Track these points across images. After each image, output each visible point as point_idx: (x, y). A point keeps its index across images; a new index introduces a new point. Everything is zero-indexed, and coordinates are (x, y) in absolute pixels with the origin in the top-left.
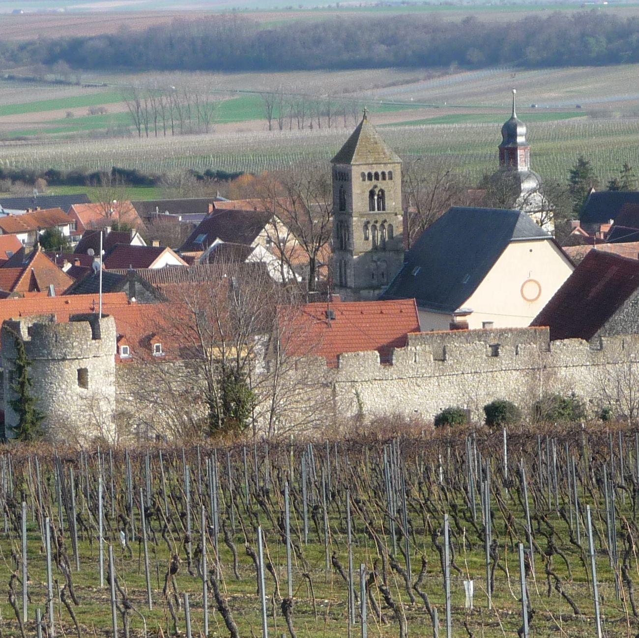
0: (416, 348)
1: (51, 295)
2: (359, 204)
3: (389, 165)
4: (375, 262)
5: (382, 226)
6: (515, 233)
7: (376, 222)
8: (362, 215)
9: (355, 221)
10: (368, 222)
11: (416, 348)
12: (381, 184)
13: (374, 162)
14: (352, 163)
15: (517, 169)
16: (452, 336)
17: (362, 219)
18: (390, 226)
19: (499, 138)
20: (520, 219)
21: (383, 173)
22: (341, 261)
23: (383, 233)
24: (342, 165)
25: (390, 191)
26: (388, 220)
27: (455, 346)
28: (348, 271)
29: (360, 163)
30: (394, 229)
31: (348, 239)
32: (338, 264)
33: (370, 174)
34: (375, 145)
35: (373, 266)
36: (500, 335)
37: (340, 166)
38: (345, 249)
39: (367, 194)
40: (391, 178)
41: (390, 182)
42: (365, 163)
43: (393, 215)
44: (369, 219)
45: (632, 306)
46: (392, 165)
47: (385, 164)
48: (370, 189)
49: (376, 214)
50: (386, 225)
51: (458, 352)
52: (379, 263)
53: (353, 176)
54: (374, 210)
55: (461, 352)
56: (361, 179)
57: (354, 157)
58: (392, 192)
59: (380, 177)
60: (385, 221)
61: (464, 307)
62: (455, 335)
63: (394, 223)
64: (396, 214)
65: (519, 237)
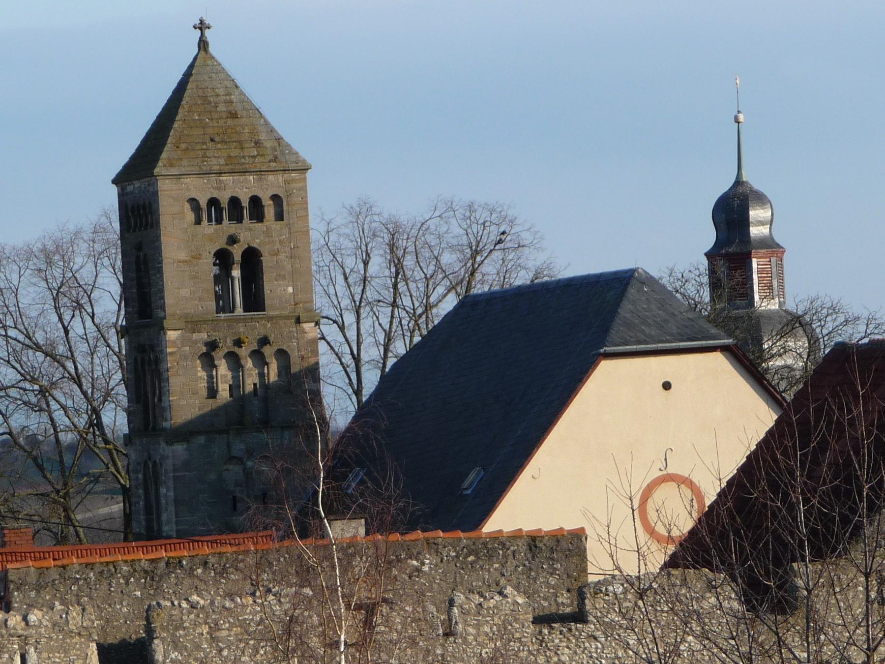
0: (25, 619)
2: (185, 292)
3: (271, 178)
4: (240, 461)
6: (617, 330)
7: (238, 343)
8: (192, 324)
9: (174, 342)
10: (212, 345)
11: (25, 619)
13: (226, 168)
14: (157, 171)
16: (191, 572)
17: (195, 336)
18: (282, 354)
19: (708, 237)
21: (255, 202)
22: (146, 463)
24: (137, 184)
25: (277, 253)
26: (271, 339)
27: (193, 606)
28: (163, 490)
31: (160, 400)
32: (140, 476)
34: (230, 122)
37: (136, 186)
38: (154, 429)
39: (207, 261)
40: (279, 216)
41: (277, 226)
44: (215, 336)
46: (280, 178)
48: (221, 244)
50: (268, 351)
51: (205, 629)
53: (162, 210)
55: (216, 627)
56: (190, 216)
57: (164, 155)
58: (282, 256)
60: (264, 341)
62: (205, 564)
64: (298, 321)
65: (626, 344)
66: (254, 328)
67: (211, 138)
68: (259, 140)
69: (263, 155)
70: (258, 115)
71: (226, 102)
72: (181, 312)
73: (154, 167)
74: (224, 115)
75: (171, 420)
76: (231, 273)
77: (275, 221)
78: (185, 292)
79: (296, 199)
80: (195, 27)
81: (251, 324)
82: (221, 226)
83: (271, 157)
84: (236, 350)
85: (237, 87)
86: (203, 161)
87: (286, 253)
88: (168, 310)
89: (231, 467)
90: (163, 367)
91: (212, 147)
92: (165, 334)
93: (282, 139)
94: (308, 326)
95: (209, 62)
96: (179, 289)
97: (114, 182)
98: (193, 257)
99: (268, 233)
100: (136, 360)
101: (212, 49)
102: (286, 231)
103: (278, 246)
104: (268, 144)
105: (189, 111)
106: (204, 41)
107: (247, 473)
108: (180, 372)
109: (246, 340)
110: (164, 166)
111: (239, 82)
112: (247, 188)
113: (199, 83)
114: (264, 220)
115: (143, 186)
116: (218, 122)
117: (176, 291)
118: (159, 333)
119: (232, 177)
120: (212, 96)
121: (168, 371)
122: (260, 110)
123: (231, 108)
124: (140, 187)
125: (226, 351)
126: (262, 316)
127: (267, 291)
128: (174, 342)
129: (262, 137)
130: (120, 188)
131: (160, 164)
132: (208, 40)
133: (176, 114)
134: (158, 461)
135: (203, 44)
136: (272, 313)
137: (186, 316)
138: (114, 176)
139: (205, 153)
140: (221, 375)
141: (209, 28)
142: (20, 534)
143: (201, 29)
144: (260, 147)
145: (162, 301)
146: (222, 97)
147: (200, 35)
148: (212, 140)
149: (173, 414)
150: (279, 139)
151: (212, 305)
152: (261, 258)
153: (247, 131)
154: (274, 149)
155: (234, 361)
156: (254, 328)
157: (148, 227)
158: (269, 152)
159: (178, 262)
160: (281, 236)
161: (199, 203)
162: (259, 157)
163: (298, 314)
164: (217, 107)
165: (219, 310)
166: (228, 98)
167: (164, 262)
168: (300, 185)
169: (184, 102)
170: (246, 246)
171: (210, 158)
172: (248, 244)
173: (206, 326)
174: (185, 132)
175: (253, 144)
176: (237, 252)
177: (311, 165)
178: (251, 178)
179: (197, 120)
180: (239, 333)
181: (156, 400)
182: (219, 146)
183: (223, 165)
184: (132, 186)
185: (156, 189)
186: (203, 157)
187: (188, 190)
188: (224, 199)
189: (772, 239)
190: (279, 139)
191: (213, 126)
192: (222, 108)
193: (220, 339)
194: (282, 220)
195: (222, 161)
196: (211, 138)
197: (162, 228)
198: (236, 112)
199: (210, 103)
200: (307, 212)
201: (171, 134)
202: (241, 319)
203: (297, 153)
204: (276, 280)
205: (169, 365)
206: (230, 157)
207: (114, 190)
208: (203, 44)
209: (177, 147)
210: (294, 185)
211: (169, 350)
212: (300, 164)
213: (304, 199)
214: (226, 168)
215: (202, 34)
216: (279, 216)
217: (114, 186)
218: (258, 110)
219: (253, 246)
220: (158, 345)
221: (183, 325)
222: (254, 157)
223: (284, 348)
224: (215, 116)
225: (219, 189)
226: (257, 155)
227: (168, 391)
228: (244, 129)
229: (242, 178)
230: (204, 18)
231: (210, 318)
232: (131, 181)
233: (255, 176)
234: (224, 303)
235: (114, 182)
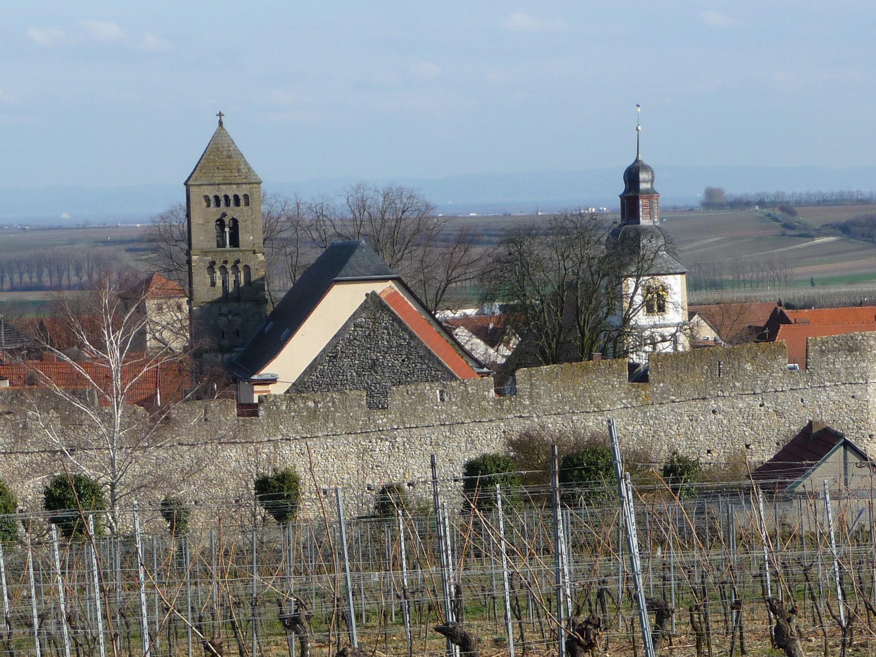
1: (440, 392)
2: (202, 238)
3: (244, 186)
5: (235, 267)
6: (346, 269)
7: (226, 262)
8: (205, 253)
9: (195, 261)
10: (213, 263)
12: (233, 212)
13: (222, 182)
15: (639, 223)
18: (247, 267)
19: (621, 187)
20: (357, 251)
21: (236, 198)
23: (237, 277)
26: (241, 260)
29: (201, 182)
30: (252, 271)
33: (217, 198)
34: (227, 160)
35: (223, 321)
36: (13, 398)
39: (213, 224)
40: (247, 204)
42: (208, 182)
43: (252, 252)
45: (330, 361)
47: (238, 184)
48: (218, 217)
49: (226, 251)
50: (240, 266)
52: (230, 317)
54: (224, 246)
56: (205, 204)
59: (232, 202)
60: (238, 261)
61: (268, 371)
63: (251, 264)
64: (254, 252)
76: (224, 229)
78: (202, 238)
80: (217, 115)
83: (245, 177)
84: (224, 265)
85: (234, 143)
89: (221, 318)
95: (222, 132)
99: (242, 211)
101: (224, 125)
102: (250, 211)
103: (246, 217)
105: (209, 155)
107: (229, 321)
127: (240, 238)
129: (242, 167)
135: (221, 123)
136: (242, 248)
148: (218, 168)
151: (215, 244)
155: (223, 269)
158: (244, 174)
165: (219, 246)
176: (227, 220)
188: (221, 196)
189: (653, 189)
190: (249, 169)
192: (225, 153)
194: (248, 205)
206: (224, 176)
208: (221, 123)
211: (193, 264)
216: (247, 204)
222: (236, 177)
225: (219, 191)
229: (230, 186)
231: (213, 250)
234: (221, 244)
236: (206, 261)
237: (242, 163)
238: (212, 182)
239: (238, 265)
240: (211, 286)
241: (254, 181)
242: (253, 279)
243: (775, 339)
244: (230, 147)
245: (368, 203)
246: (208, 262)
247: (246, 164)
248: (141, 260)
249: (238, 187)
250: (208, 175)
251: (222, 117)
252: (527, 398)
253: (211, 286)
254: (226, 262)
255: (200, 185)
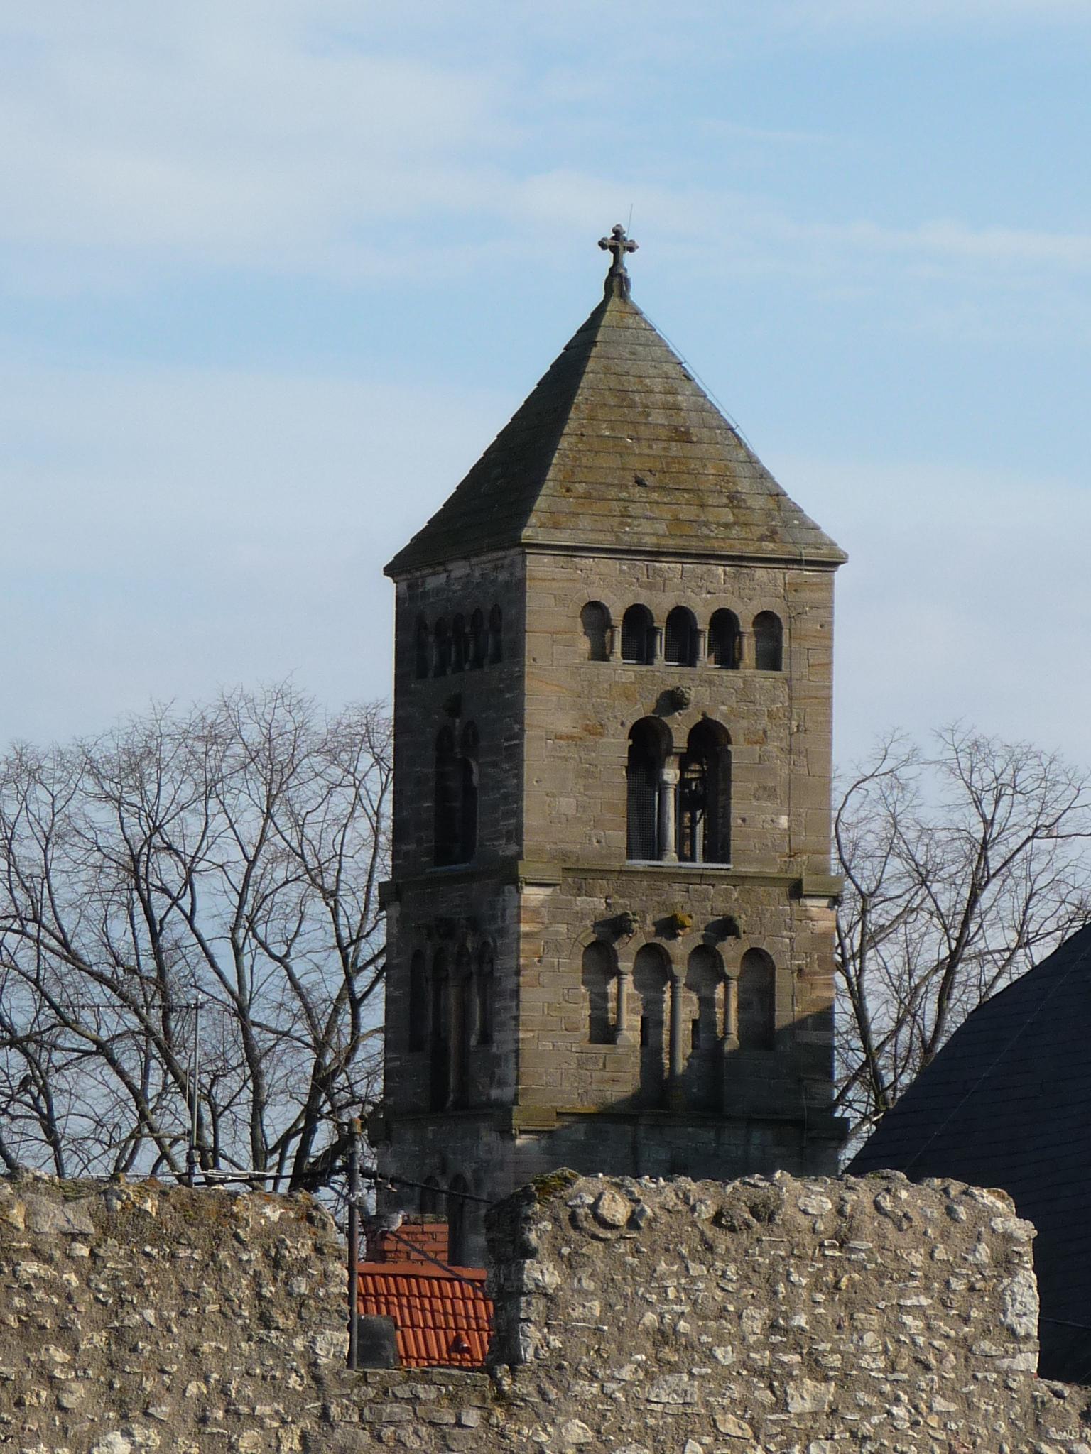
2: (566, 804)
3: (761, 573)
5: (706, 956)
7: (670, 927)
10: (616, 927)
13: (671, 544)
14: (527, 533)
17: (581, 902)
23: (707, 1003)
24: (459, 569)
25: (764, 738)
26: (742, 923)
29: (581, 539)
30: (784, 982)
31: (486, 1038)
34: (675, 449)
39: (617, 746)
40: (771, 659)
41: (765, 679)
42: (607, 541)
44: (623, 904)
46: (782, 577)
47: (738, 560)
48: (642, 709)
50: (731, 951)
53: (531, 620)
56: (584, 644)
57: (540, 503)
58: (772, 747)
60: (726, 927)
63: (778, 946)
64: (796, 891)
66: (706, 897)
67: (636, 477)
68: (738, 492)
69: (745, 524)
70: (734, 442)
71: (667, 407)
72: (553, 847)
73: (522, 525)
74: (663, 433)
75: (517, 1084)
76: (660, 774)
77: (758, 668)
78: (566, 804)
79: (809, 626)
80: (602, 245)
81: (697, 886)
82: (649, 668)
83: (763, 530)
84: (662, 941)
85: (688, 378)
86: (623, 524)
87: (781, 739)
88: (529, 842)
90: (503, 964)
91: (641, 497)
92: (519, 891)
93: (785, 495)
94: (816, 906)
95: (630, 321)
96: (554, 796)
97: (390, 570)
98: (587, 729)
99: (745, 694)
100: (418, 956)
102: (782, 693)
104: (757, 503)
105: (592, 419)
106: (620, 276)
108: (545, 979)
109: (688, 922)
110: (542, 526)
111: (692, 367)
112: (709, 593)
113: (610, 361)
114: (742, 665)
115: (477, 574)
116: (650, 447)
117: (548, 799)
118: (499, 892)
119: (679, 566)
120: (638, 391)
121: (518, 973)
122: (737, 431)
123: (678, 421)
124: (468, 575)
125: (644, 942)
126: (723, 873)
128: (536, 911)
129: (744, 486)
130: (404, 585)
131: (533, 520)
132: (630, 275)
133: (562, 419)
134: (468, 1175)
135: (616, 282)
137: (565, 856)
138: (389, 558)
139: (626, 508)
140: (628, 994)
141: (631, 249)
142: (420, 1237)
143: (614, 249)
144: (739, 507)
145: (513, 821)
146: (658, 396)
147: (611, 264)
148: (639, 482)
149: (521, 1070)
150: (778, 495)
151: (619, 838)
152: (729, 747)
153: (712, 471)
154: (769, 514)
156: (706, 897)
157: (486, 661)
159: (556, 737)
160: (773, 701)
161: (609, 613)
162: (737, 528)
163: (798, 876)
164: (648, 415)
166: (670, 398)
167: (527, 734)
168: (819, 596)
169: (579, 399)
170: (700, 718)
171: (636, 518)
172: (704, 714)
173: (605, 882)
174: (584, 461)
175: (725, 500)
176: (680, 728)
177: (847, 555)
178: (720, 569)
179: (608, 437)
180: (673, 905)
181: (473, 1041)
182: (655, 496)
183: (664, 536)
184: (445, 575)
185: (518, 574)
186: (622, 516)
187: (589, 583)
191: (640, 455)
193: (634, 914)
194: (776, 666)
195: (661, 528)
196: (636, 477)
197: (528, 661)
198: (688, 428)
199: (632, 405)
200: (830, 656)
201: (554, 461)
202: (679, 874)
203: (816, 528)
204: (757, 798)
205: (522, 961)
207: (389, 589)
208: (616, 282)
209: (568, 490)
210: (806, 595)
212: (824, 551)
213: (826, 628)
214: (671, 542)
215: (617, 261)
217: (390, 579)
218: (732, 429)
219: (713, 718)
220: (493, 918)
221: (557, 876)
222: (727, 526)
223: (764, 948)
224: (644, 432)
225: (650, 587)
226: (735, 523)
227: (516, 1018)
228: (704, 466)
230: (625, 228)
232: (442, 564)
233: (728, 569)
235: (390, 570)
236: (581, 916)
237: (740, 469)
238: (627, 540)
239: (720, 946)
240: (594, 1039)
241: (808, 553)
242: (783, 1018)
243: (1035, 1272)
244: (674, 392)
245: (96, 755)
246: (588, 923)
247: (762, 476)
248: (11, 891)
249: (737, 577)
250: (599, 507)
251: (627, 258)
252: (38, 1351)
253: (594, 1039)
254: (670, 927)
255: (572, 551)
